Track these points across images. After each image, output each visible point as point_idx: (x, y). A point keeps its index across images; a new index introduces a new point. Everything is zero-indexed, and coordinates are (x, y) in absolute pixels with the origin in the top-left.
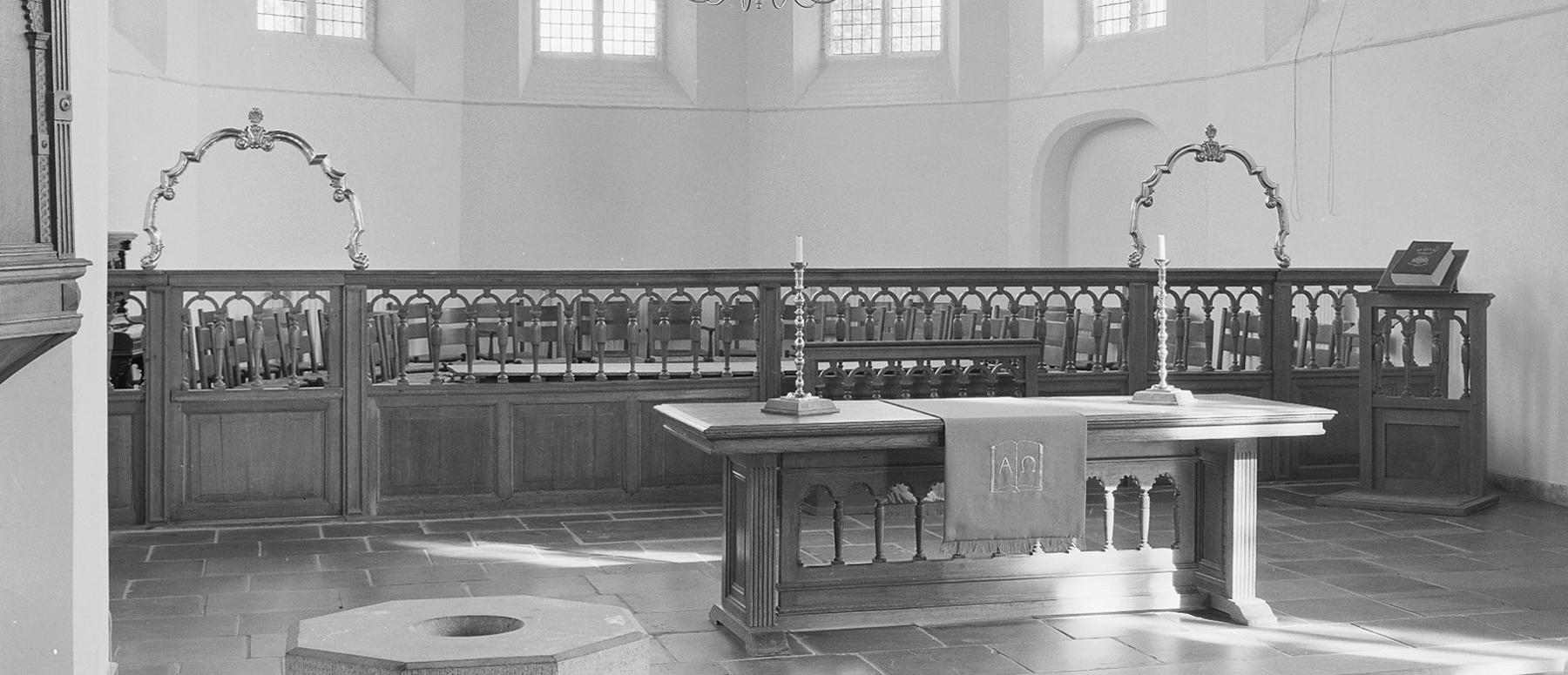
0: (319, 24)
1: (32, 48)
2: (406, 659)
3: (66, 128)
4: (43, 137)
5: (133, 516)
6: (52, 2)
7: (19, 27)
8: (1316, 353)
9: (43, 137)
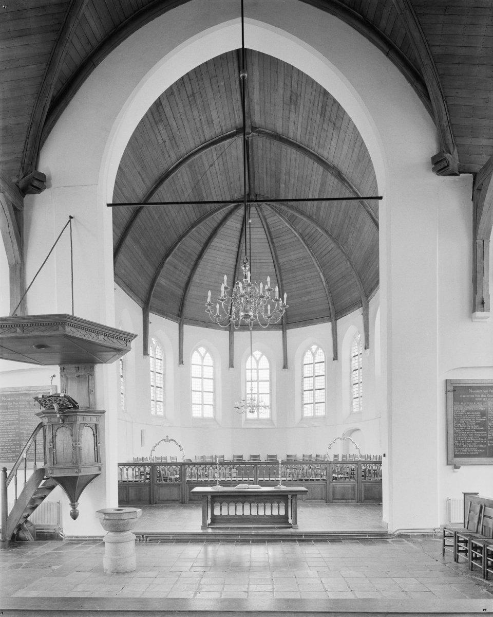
1: (94, 436)
4: (96, 448)
9: (96, 448)
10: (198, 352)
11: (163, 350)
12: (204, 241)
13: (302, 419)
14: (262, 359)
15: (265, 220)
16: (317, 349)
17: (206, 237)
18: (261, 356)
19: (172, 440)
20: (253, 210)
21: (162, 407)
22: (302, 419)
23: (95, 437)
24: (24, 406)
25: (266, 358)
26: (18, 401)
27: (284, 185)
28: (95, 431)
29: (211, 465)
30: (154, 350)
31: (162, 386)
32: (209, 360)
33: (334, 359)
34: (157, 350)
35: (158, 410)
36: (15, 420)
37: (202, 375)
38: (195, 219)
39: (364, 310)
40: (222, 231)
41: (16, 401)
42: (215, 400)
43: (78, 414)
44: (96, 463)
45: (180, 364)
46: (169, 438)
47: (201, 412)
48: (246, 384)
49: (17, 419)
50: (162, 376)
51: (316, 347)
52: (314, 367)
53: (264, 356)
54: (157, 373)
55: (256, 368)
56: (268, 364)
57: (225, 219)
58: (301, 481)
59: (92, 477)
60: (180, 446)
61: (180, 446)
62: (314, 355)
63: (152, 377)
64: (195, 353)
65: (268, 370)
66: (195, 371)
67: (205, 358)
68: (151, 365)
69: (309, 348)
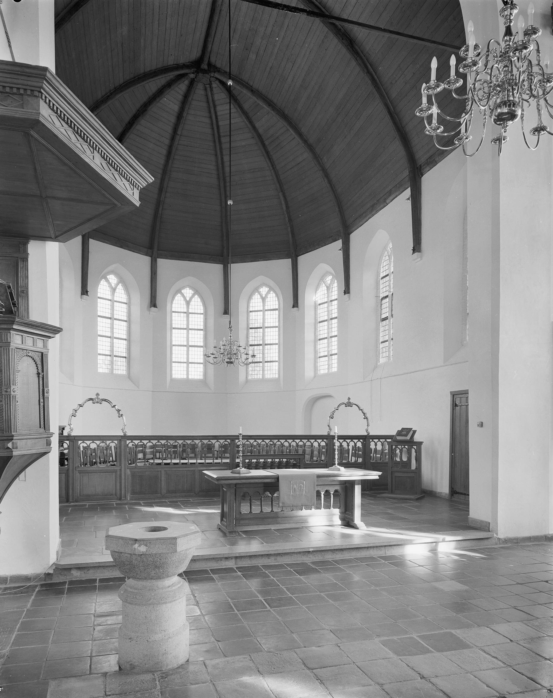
1: (39, 377)
4: (42, 400)
9: (42, 400)
10: (107, 281)
12: (127, 118)
13: (247, 381)
14: (193, 299)
15: (215, 107)
16: (268, 292)
17: (131, 115)
19: (105, 400)
20: (199, 91)
22: (247, 381)
23: (41, 379)
25: (199, 300)
27: (254, 57)
29: (201, 440)
32: (121, 294)
33: (294, 307)
37: (112, 314)
38: (122, 81)
39: (343, 243)
40: (154, 109)
42: (129, 349)
43: (15, 327)
44: (42, 430)
45: (83, 293)
46: (101, 397)
48: (171, 331)
51: (267, 289)
52: (264, 315)
53: (196, 296)
55: (185, 311)
56: (202, 308)
57: (160, 93)
58: (158, 466)
59: (35, 457)
60: (119, 411)
61: (119, 411)
62: (264, 299)
64: (103, 282)
65: (202, 316)
66: (103, 308)
67: (117, 290)
69: (256, 290)
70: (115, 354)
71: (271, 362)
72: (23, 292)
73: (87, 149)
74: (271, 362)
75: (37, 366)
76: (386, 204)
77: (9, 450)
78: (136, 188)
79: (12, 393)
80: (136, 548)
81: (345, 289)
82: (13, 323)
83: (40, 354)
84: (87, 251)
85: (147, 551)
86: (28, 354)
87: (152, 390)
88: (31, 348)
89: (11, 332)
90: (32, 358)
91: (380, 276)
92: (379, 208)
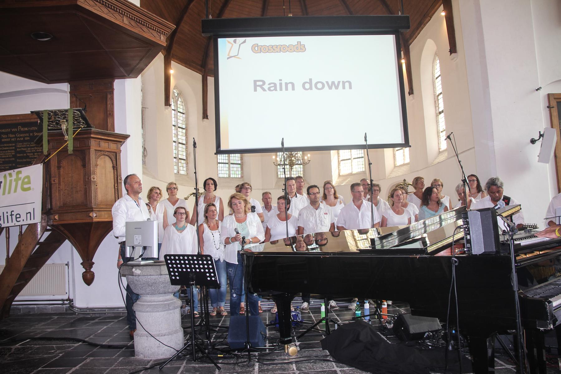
0: (231, 175)
1: (114, 169)
2: (539, 153)
3: (465, 204)
4: (116, 185)
5: (110, 212)
6: (560, 249)
7: (111, 165)
8: (371, 314)
9: (116, 185)
11: (185, 102)
18: (383, 246)
21: (185, 165)
24: (22, 139)
26: (14, 133)
28: (114, 162)
30: (176, 102)
31: (184, 142)
34: (179, 103)
35: (181, 168)
36: (10, 158)
41: (12, 133)
43: (92, 136)
47: (227, 172)
49: (14, 156)
50: (184, 146)
54: (179, 127)
63: (174, 132)
68: (173, 119)
70: (231, 162)
71: (360, 158)
72: (110, 114)
73: (117, 15)
74: (360, 158)
75: (112, 162)
76: (429, 18)
77: (90, 218)
78: (163, 34)
79: (92, 180)
80: (134, 271)
81: (409, 91)
82: (90, 133)
83: (115, 154)
84: (206, 90)
85: (141, 273)
86: (105, 154)
87: (261, 188)
88: (107, 149)
89: (91, 139)
90: (108, 156)
91: (435, 77)
92: (425, 22)
